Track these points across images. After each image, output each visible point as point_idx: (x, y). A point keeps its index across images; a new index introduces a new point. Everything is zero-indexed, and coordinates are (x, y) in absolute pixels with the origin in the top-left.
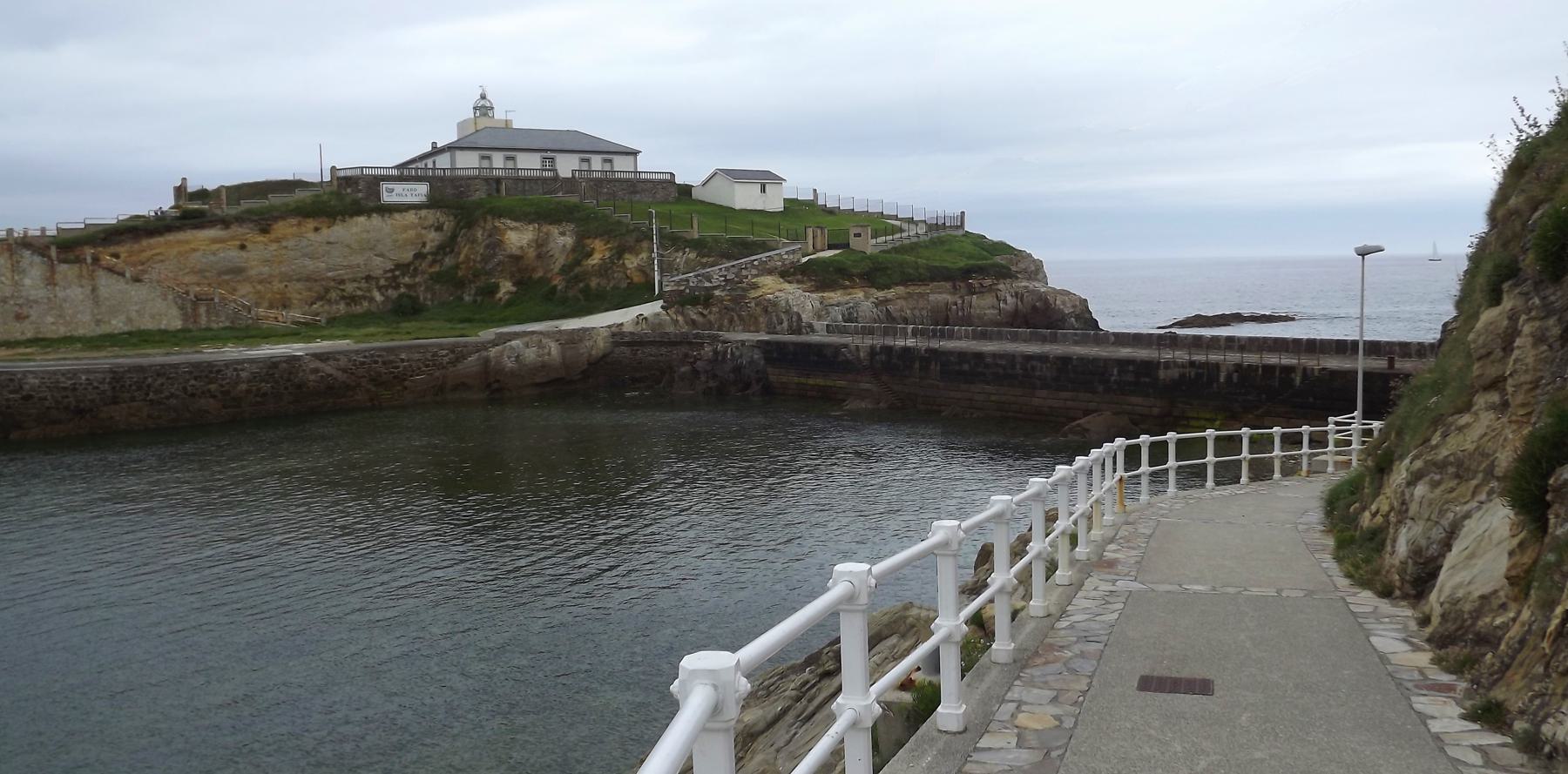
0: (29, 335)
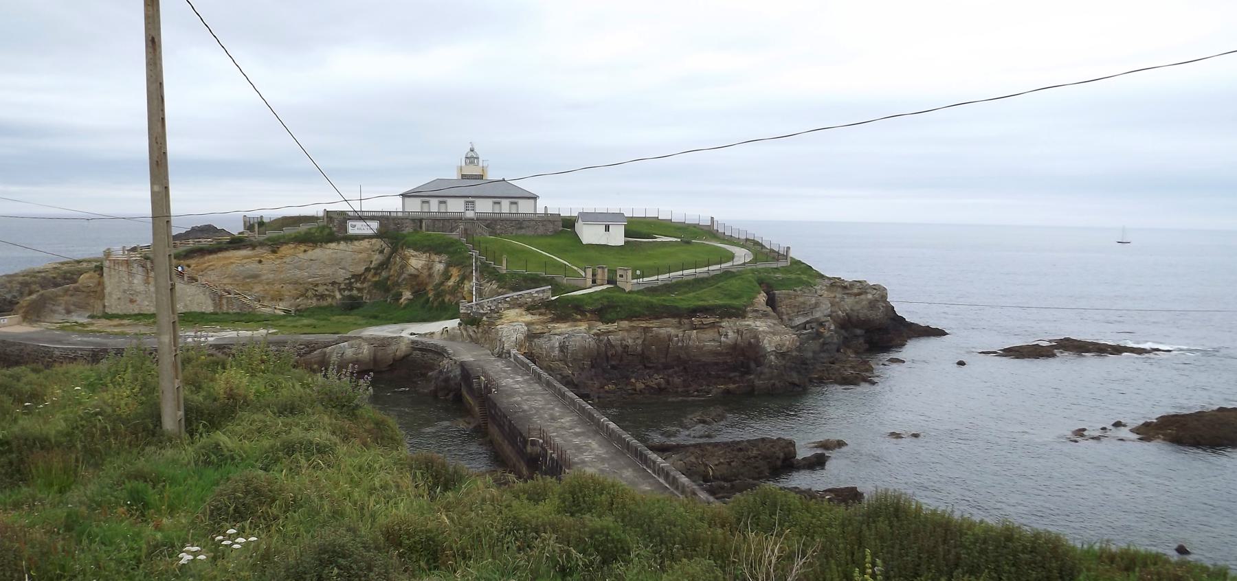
0: (136, 312)
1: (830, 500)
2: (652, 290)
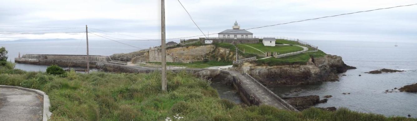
0: (156, 62)
1: (328, 110)
2: (282, 58)
